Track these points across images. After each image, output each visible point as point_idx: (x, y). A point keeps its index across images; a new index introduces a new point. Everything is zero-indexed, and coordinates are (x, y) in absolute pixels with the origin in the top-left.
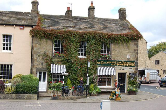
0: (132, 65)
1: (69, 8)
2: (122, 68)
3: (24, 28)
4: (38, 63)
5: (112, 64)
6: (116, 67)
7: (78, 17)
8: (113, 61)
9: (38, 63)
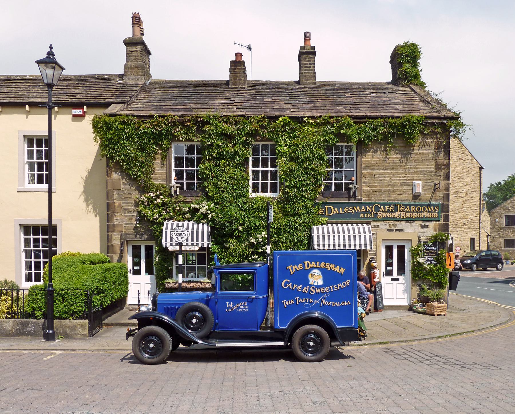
0: (430, 215)
1: (238, 55)
2: (395, 226)
3: (84, 112)
4: (125, 220)
5: (362, 215)
6: (374, 224)
7: (266, 81)
8: (366, 205)
9: (125, 220)
